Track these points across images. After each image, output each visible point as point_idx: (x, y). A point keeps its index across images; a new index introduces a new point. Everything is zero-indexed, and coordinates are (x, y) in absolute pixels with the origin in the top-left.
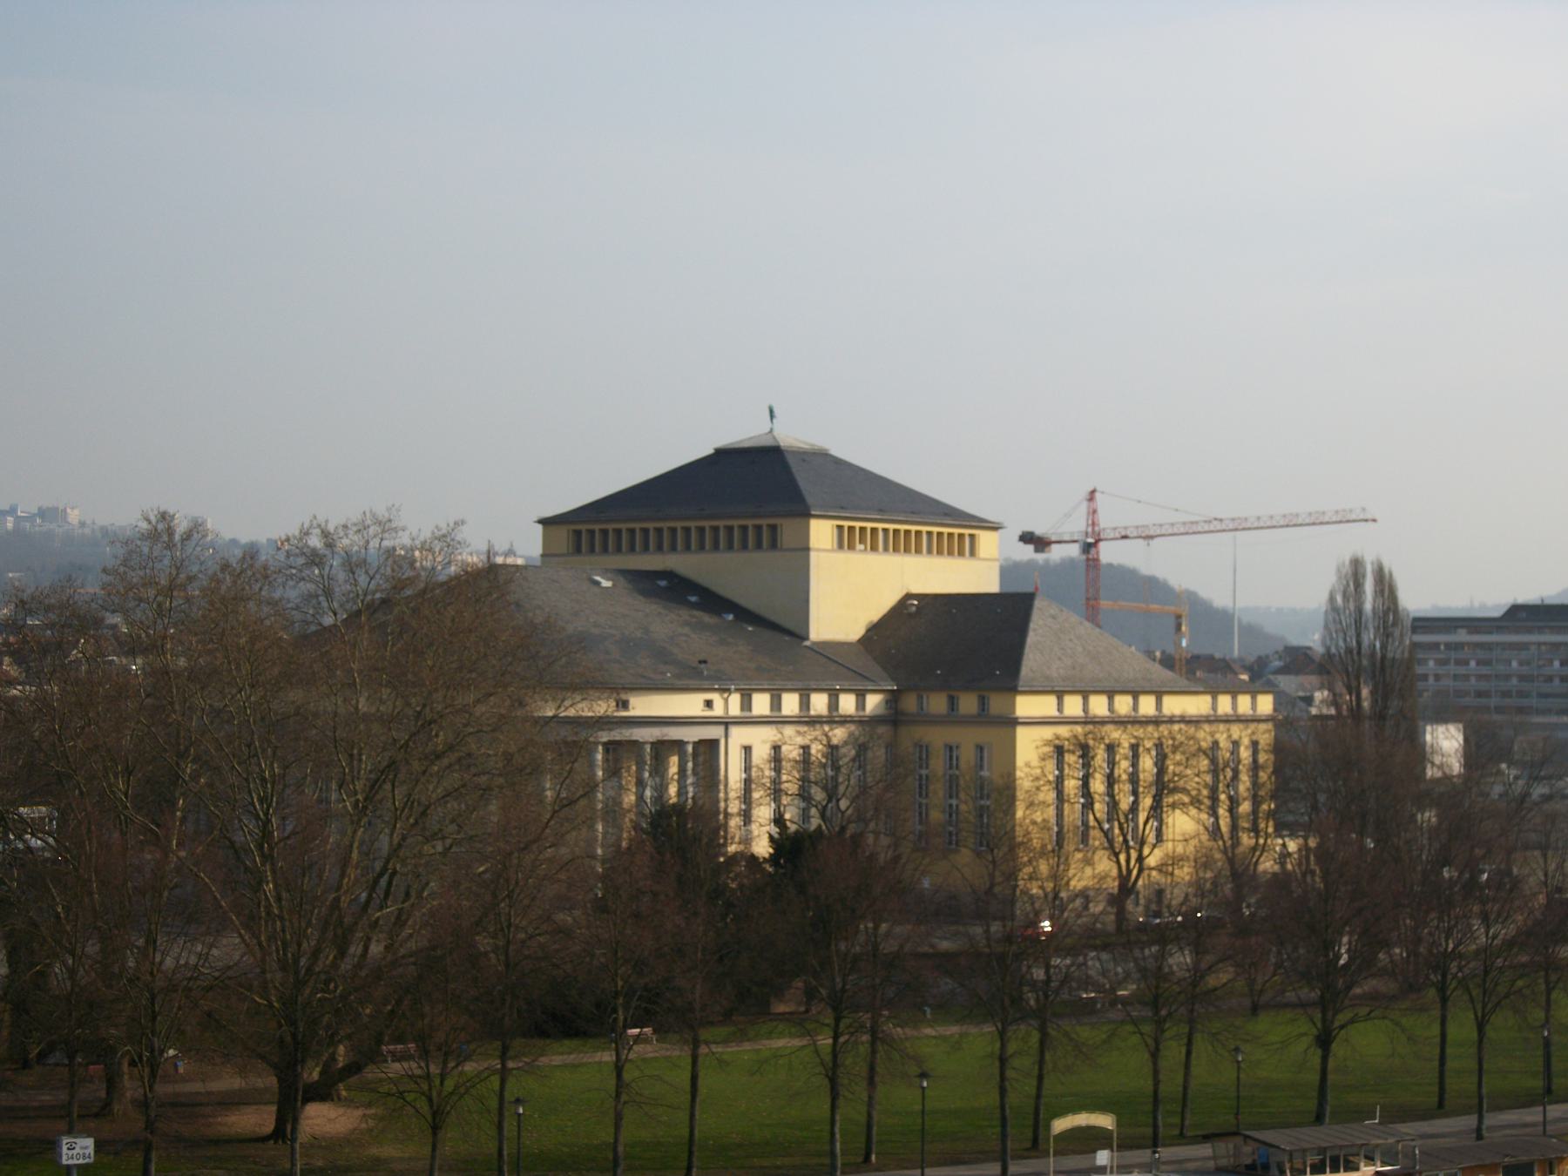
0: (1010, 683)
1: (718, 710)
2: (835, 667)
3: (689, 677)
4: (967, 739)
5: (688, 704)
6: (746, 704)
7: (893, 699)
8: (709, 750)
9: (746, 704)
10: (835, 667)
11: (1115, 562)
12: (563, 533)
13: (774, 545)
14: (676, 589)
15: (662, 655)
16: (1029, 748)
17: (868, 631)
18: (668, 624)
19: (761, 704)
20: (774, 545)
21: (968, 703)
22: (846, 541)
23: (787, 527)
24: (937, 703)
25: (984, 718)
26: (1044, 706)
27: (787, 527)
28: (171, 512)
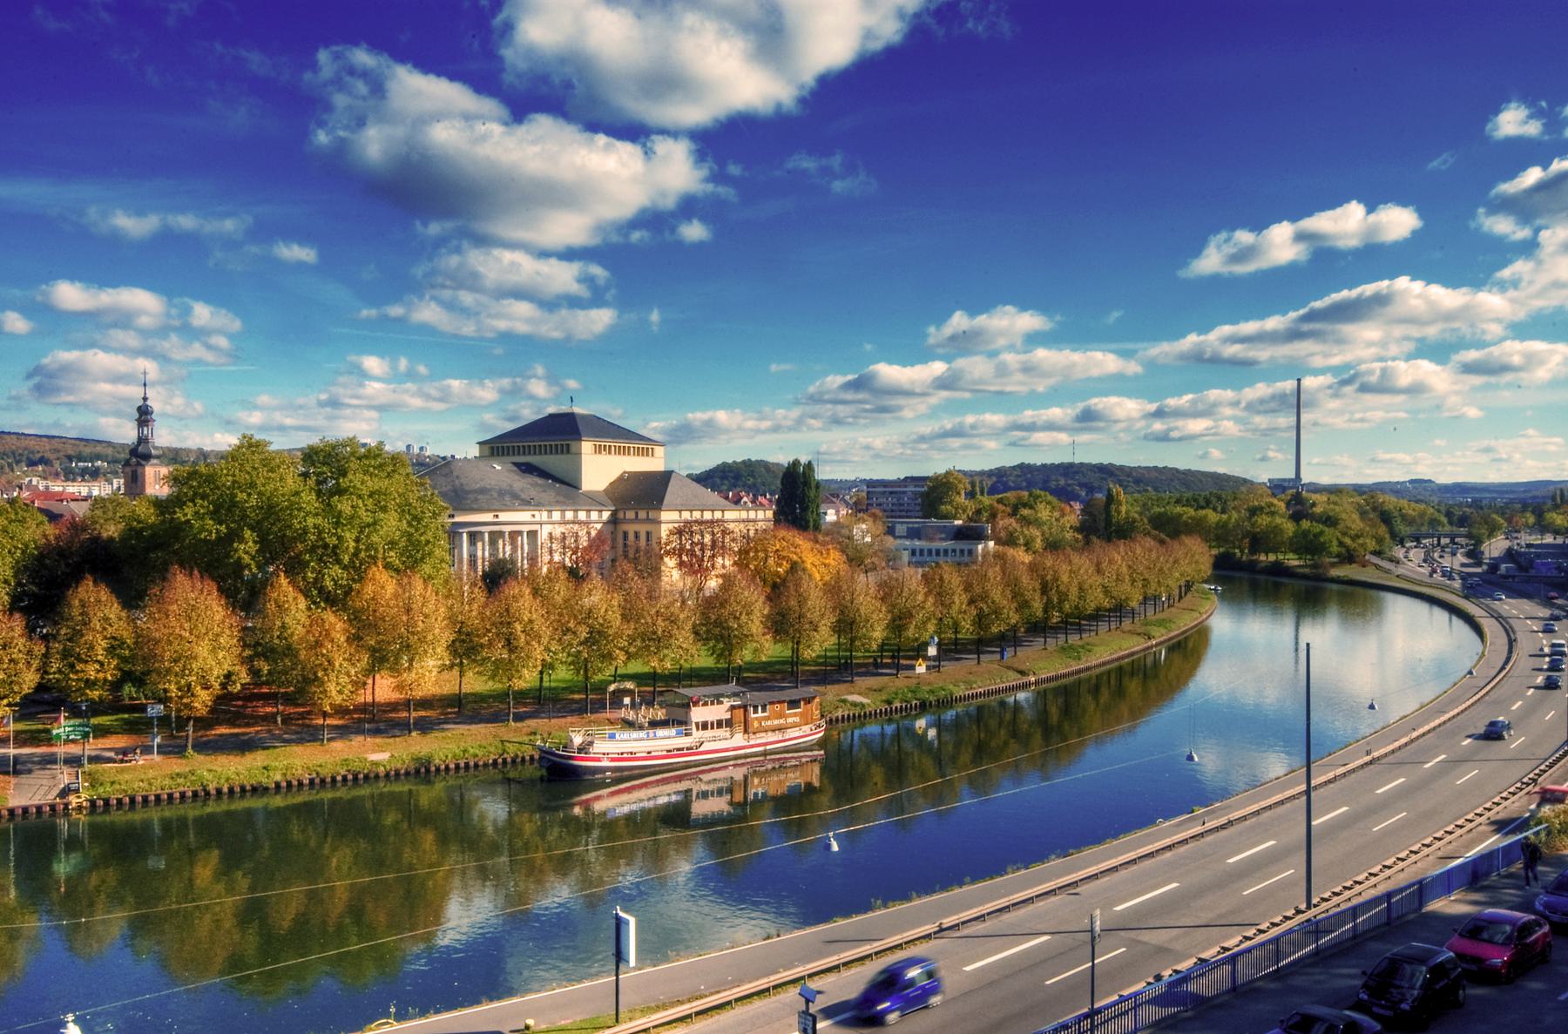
0: (659, 508)
1: (537, 518)
2: (593, 500)
3: (527, 504)
4: (643, 529)
5: (524, 516)
6: (550, 516)
7: (614, 513)
8: (533, 535)
9: (550, 516)
10: (593, 500)
11: (1106, 462)
12: (487, 448)
13: (568, 452)
14: (527, 469)
15: (515, 496)
16: (664, 530)
17: (744, 462)
18: (522, 483)
19: (556, 516)
20: (568, 452)
21: (642, 515)
22: (598, 450)
23: (573, 444)
24: (630, 515)
25: (648, 520)
26: (674, 516)
27: (573, 444)
28: (804, 460)
